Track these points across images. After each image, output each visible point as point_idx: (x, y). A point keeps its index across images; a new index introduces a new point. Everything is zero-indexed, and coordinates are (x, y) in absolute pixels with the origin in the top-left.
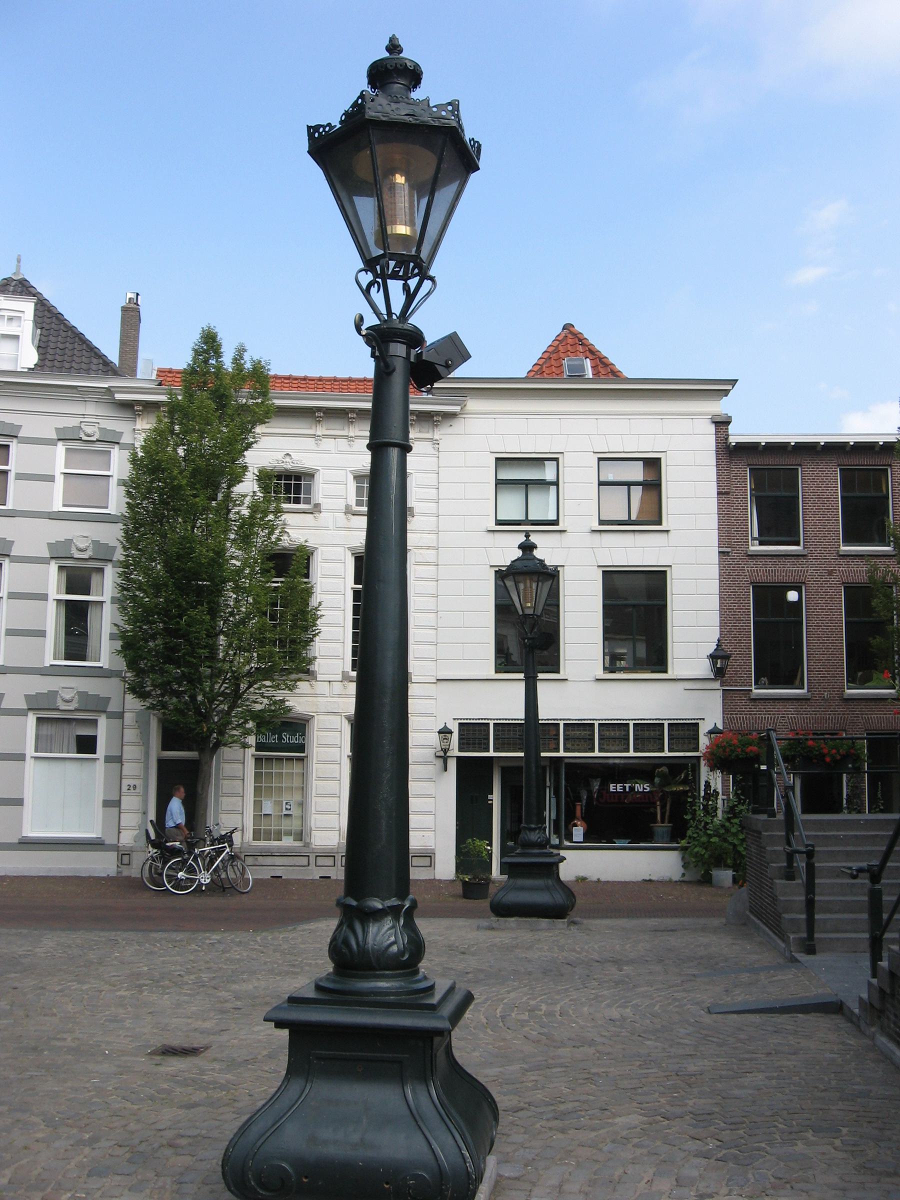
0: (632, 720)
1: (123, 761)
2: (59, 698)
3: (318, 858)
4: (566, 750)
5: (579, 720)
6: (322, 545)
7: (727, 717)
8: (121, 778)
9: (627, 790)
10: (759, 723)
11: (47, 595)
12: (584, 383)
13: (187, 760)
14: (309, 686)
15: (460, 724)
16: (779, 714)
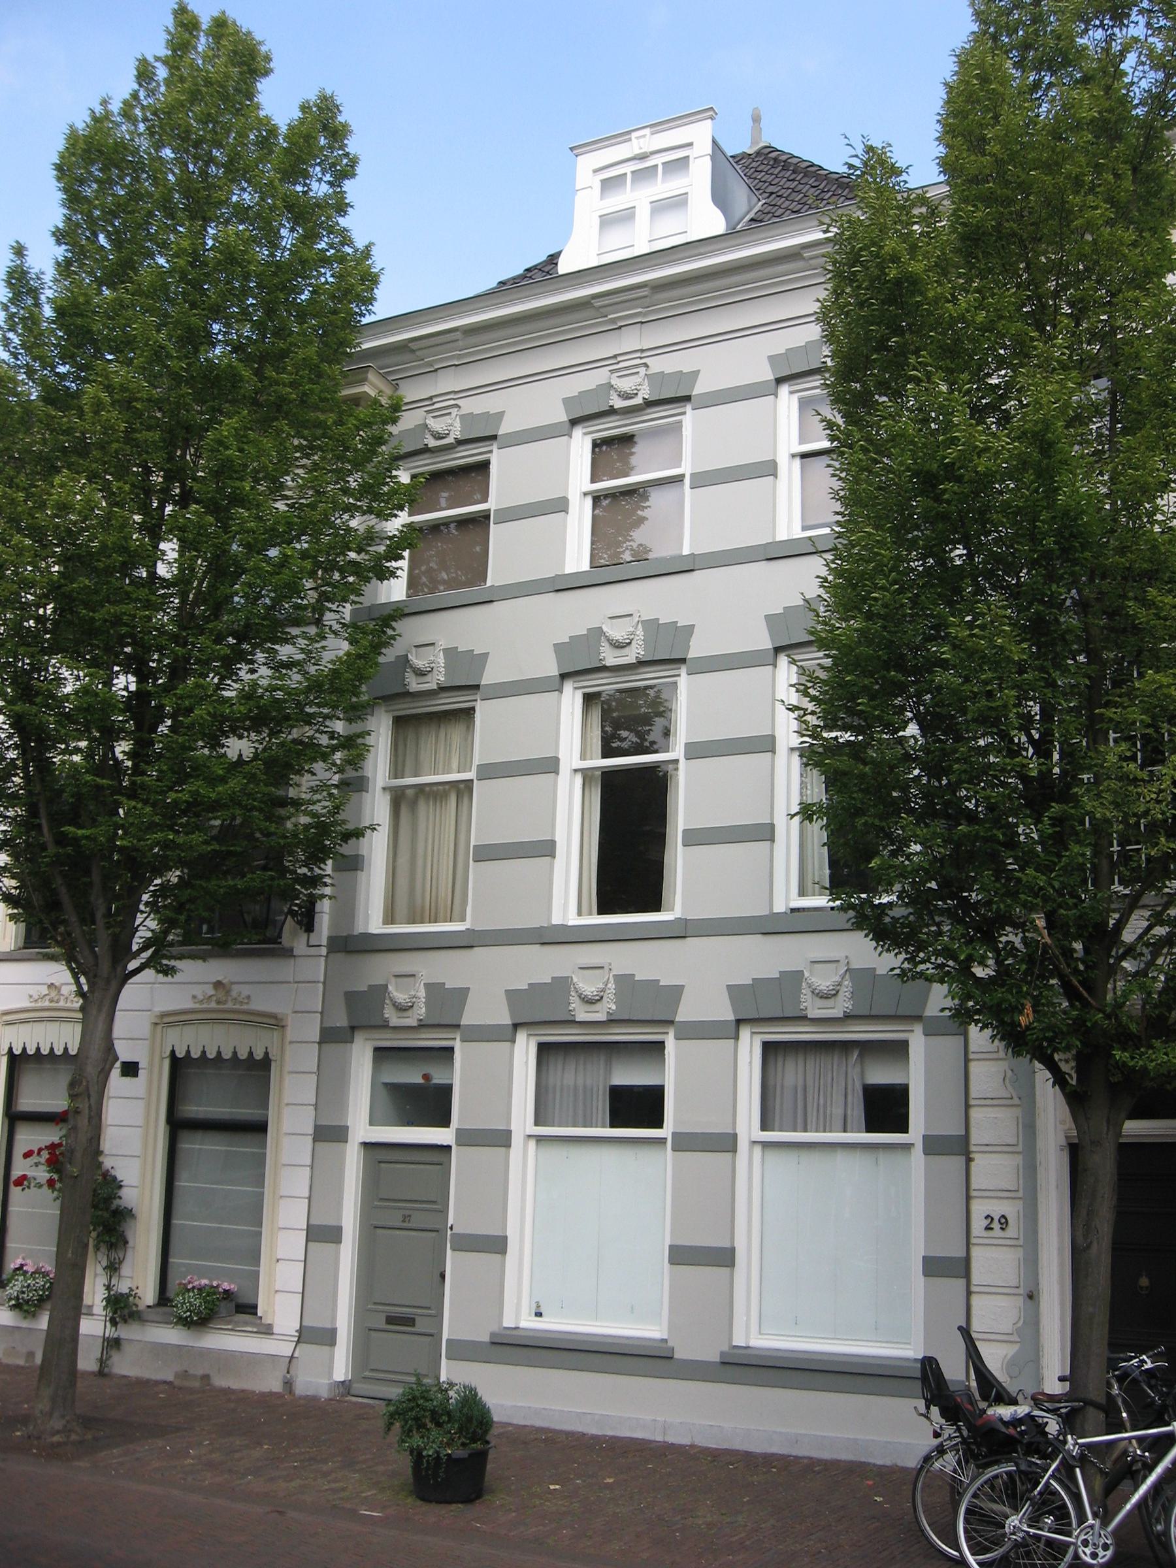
1: (973, 1148)
2: (805, 990)
8: (968, 1198)
11: (772, 738)
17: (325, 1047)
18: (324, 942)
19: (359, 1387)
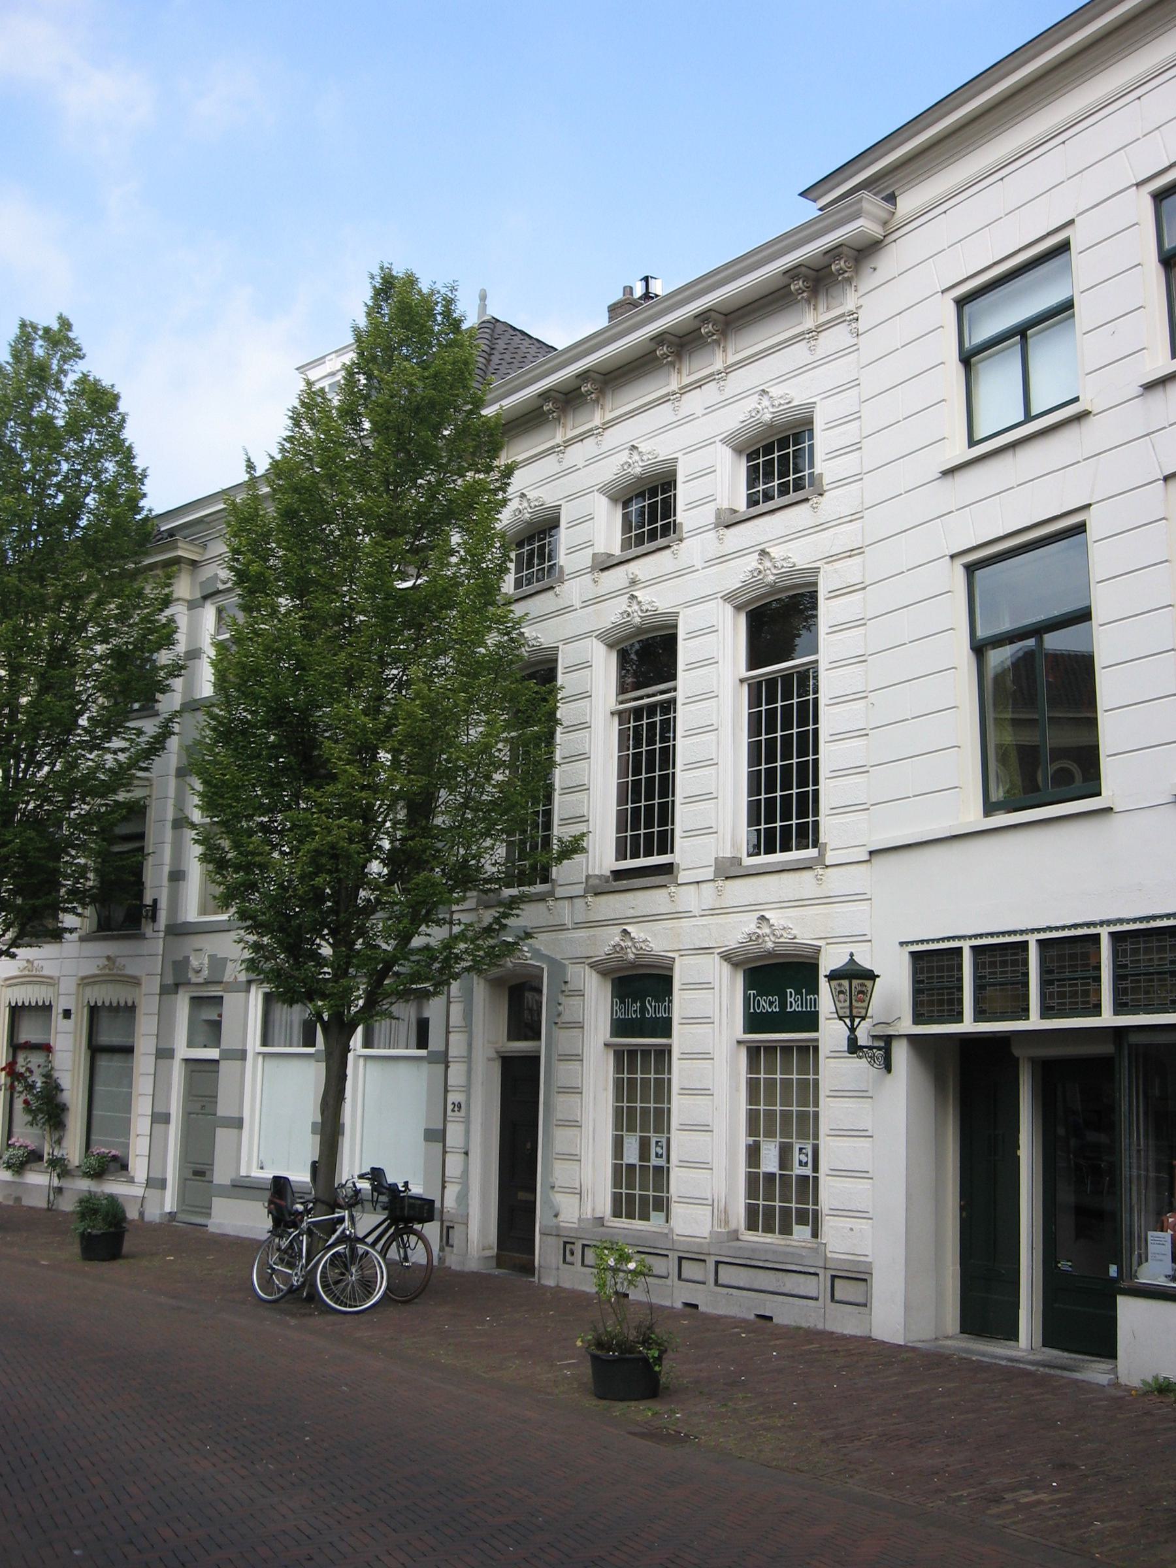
0: (1033, 931)
3: (721, 1266)
4: (980, 1015)
6: (567, 641)
12: (896, 148)
14: (545, 910)
15: (913, 954)
17: (164, 997)
18: (162, 928)
19: (180, 1217)
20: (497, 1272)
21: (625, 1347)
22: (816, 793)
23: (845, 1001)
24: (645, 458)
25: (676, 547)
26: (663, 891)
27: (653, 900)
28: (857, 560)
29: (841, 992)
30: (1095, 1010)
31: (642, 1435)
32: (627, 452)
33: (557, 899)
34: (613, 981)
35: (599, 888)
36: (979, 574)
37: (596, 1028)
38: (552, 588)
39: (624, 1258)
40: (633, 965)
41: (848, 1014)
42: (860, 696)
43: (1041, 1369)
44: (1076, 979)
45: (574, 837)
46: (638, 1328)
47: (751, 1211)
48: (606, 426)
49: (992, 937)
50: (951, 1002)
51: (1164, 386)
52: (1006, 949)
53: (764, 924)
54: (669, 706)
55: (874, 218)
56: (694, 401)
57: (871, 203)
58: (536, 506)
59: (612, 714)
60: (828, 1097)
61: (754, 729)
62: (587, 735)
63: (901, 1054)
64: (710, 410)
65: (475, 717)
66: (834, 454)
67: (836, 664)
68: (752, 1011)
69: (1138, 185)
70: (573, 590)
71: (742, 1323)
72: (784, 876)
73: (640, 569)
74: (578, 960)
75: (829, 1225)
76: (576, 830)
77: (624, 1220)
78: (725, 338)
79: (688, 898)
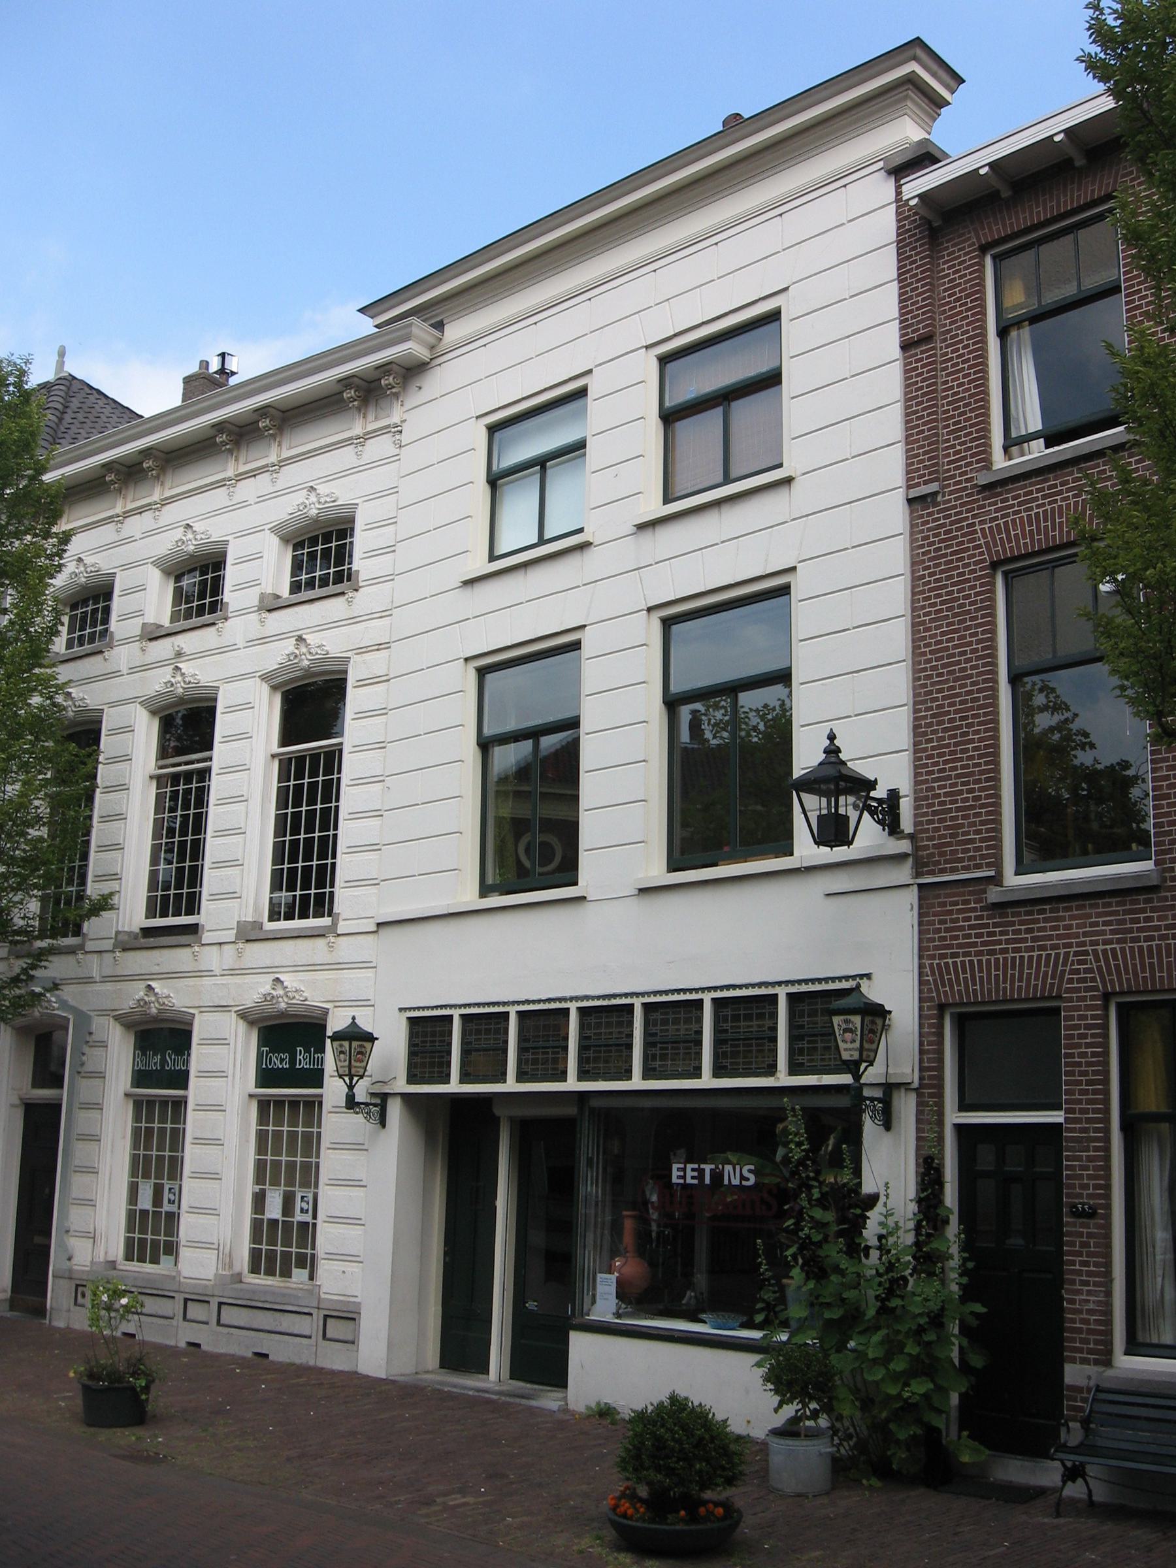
0: (709, 989)
5: (604, 997)
6: (113, 704)
7: (931, 965)
9: (707, 1180)
10: (1046, 973)
13: (47, 1104)
15: (411, 1020)
16: (1070, 945)
20: (9, 1314)
21: (115, 1377)
22: (334, 865)
23: (345, 1061)
24: (198, 537)
25: (221, 625)
26: (187, 951)
27: (178, 958)
28: (383, 654)
29: (342, 1052)
30: (562, 1076)
31: (124, 1457)
32: (182, 529)
33: (87, 952)
34: (136, 1033)
35: (128, 944)
36: (489, 677)
37: (117, 1078)
38: (101, 652)
39: (117, 1294)
40: (155, 1019)
41: (347, 1073)
42: (378, 779)
43: (503, 1398)
44: (548, 1048)
45: (103, 896)
46: (128, 1360)
47: (255, 1255)
48: (165, 502)
49: (679, 994)
50: (441, 1064)
51: (654, 528)
52: (491, 1019)
53: (279, 986)
54: (205, 774)
55: (421, 342)
56: (248, 489)
57: (419, 327)
58: (92, 572)
59: (151, 777)
60: (329, 1149)
61: (282, 802)
62: (125, 796)
63: (395, 1110)
64: (262, 499)
65: (13, 775)
66: (372, 554)
67: (359, 748)
68: (264, 1066)
69: (647, 347)
70: (122, 656)
71: (241, 1361)
72: (300, 942)
73: (186, 642)
74: (103, 1013)
75: (325, 1268)
76: (106, 888)
77: (135, 1263)
78: (281, 434)
79: (211, 958)
